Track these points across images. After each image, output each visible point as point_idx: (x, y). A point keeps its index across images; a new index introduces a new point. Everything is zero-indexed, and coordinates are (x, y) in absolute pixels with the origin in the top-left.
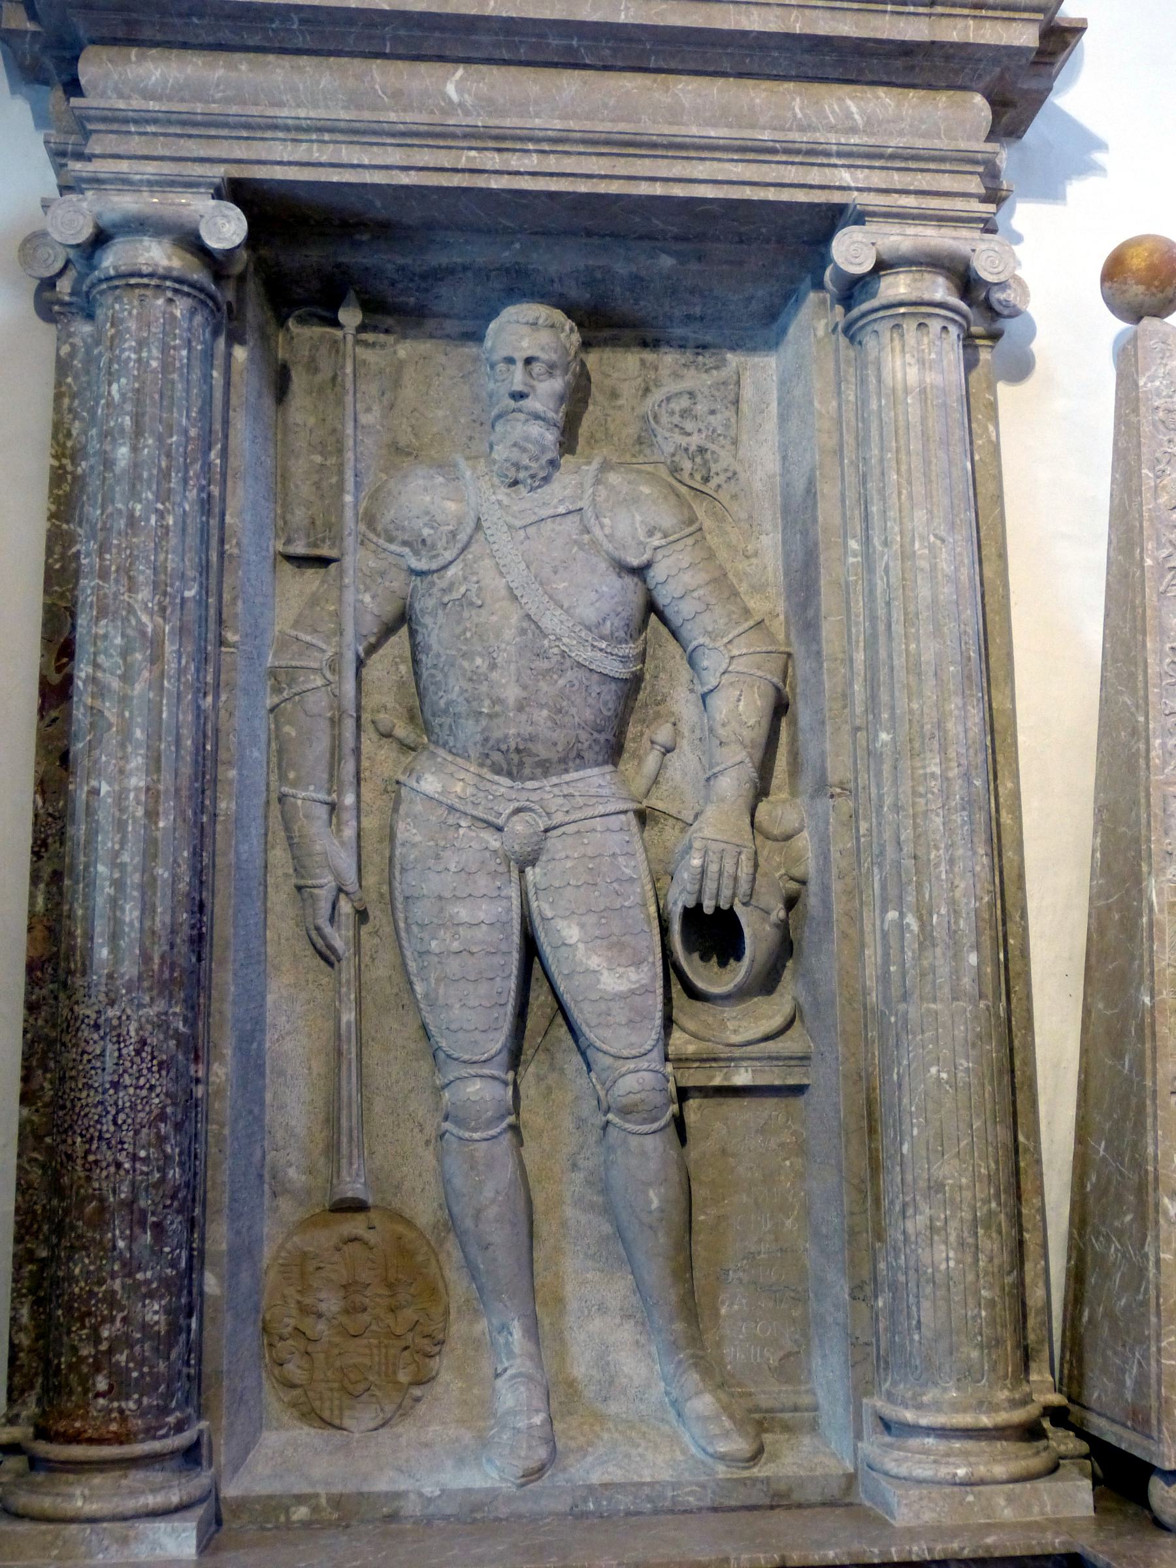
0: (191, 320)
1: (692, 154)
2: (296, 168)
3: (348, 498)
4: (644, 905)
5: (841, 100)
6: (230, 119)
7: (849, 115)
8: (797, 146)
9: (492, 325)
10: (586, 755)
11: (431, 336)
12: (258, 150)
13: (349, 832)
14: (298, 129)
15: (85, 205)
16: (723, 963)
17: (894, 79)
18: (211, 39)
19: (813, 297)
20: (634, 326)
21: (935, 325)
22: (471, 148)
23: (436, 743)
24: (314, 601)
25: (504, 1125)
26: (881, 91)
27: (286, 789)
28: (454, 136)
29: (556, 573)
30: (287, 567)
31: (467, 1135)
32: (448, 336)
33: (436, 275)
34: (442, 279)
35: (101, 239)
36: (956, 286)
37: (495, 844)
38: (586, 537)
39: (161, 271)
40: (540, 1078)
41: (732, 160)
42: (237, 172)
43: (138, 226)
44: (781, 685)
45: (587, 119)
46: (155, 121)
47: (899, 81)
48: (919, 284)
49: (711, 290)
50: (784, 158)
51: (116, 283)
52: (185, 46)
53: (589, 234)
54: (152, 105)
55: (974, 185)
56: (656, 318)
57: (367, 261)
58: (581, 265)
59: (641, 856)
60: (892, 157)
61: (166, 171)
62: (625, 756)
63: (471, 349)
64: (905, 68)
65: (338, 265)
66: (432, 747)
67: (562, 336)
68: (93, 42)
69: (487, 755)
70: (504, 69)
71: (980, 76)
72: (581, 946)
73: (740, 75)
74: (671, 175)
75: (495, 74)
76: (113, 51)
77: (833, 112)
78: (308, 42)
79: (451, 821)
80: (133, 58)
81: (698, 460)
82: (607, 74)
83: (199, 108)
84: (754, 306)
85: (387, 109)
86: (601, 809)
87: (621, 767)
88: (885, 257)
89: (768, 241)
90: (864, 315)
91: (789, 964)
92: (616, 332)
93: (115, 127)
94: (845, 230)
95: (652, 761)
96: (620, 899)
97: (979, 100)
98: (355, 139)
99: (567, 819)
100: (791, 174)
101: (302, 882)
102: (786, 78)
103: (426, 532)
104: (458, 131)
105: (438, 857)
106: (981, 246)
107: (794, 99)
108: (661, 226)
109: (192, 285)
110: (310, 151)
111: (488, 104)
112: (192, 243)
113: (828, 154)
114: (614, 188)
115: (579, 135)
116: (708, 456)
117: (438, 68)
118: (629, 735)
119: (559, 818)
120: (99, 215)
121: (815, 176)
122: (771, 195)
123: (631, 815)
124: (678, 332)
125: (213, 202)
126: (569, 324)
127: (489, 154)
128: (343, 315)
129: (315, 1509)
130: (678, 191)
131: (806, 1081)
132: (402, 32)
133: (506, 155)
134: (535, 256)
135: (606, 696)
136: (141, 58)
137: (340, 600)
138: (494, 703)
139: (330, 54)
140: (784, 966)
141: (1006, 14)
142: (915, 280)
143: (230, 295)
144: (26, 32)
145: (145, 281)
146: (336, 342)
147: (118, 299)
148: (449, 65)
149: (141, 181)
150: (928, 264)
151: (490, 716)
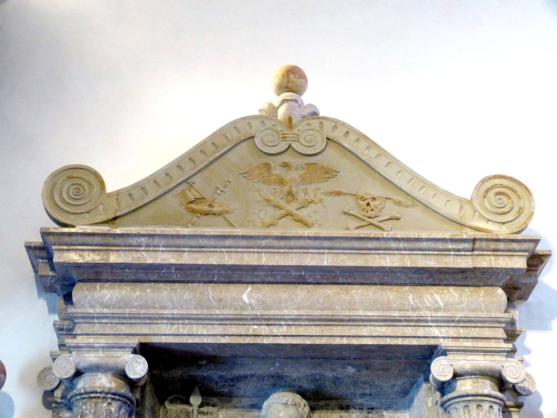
0: (119, 412)
1: (361, 323)
2: (171, 337)
5: (432, 295)
6: (142, 316)
7: (436, 302)
8: (411, 318)
9: (265, 404)
11: (236, 407)
12: (154, 329)
14: (173, 319)
15: (71, 358)
17: (457, 283)
18: (134, 278)
19: (425, 386)
20: (336, 399)
21: (486, 406)
22: (254, 325)
26: (451, 289)
28: (246, 320)
32: (244, 407)
33: (238, 379)
34: (240, 381)
35: (78, 373)
36: (497, 384)
39: (106, 390)
41: (380, 326)
42: (144, 340)
43: (96, 368)
45: (310, 309)
46: (107, 318)
47: (460, 284)
48: (476, 385)
49: (374, 382)
50: (405, 324)
51: (84, 396)
52: (122, 281)
53: (312, 358)
54: (106, 311)
55: (501, 334)
56: (347, 395)
57: (205, 374)
58: (309, 373)
60: (459, 321)
61: (110, 342)
63: (255, 413)
64: (462, 278)
65: (190, 376)
67: (300, 409)
68: (80, 281)
70: (270, 286)
71: (500, 280)
73: (382, 284)
74: (350, 334)
75: (266, 289)
76: (89, 285)
77: (428, 301)
78: (179, 277)
80: (98, 288)
82: (318, 286)
83: (127, 311)
84: (396, 389)
85: (214, 308)
88: (458, 372)
89: (401, 358)
90: (450, 400)
92: (327, 402)
93: (88, 320)
94: (437, 359)
97: (500, 291)
98: (200, 322)
100: (409, 331)
102: (405, 285)
104: (249, 317)
106: (506, 365)
107: (409, 295)
108: (347, 354)
109: (120, 395)
110: (178, 328)
111: (263, 304)
112: (122, 375)
113: (427, 321)
114: (323, 341)
115: (305, 317)
117: (239, 287)
120: (78, 364)
121: (421, 332)
122: (400, 342)
124: (359, 401)
125: (132, 355)
126: (304, 402)
127: (263, 327)
128: (192, 400)
130: (355, 342)
132: (222, 272)
133: (271, 327)
134: (286, 369)
136: (102, 288)
139: (188, 282)
141: (509, 253)
142: (474, 382)
143: (138, 395)
144: (49, 276)
145: (98, 395)
146: (188, 413)
147: (84, 404)
148: (244, 285)
149: (99, 347)
150: (480, 375)
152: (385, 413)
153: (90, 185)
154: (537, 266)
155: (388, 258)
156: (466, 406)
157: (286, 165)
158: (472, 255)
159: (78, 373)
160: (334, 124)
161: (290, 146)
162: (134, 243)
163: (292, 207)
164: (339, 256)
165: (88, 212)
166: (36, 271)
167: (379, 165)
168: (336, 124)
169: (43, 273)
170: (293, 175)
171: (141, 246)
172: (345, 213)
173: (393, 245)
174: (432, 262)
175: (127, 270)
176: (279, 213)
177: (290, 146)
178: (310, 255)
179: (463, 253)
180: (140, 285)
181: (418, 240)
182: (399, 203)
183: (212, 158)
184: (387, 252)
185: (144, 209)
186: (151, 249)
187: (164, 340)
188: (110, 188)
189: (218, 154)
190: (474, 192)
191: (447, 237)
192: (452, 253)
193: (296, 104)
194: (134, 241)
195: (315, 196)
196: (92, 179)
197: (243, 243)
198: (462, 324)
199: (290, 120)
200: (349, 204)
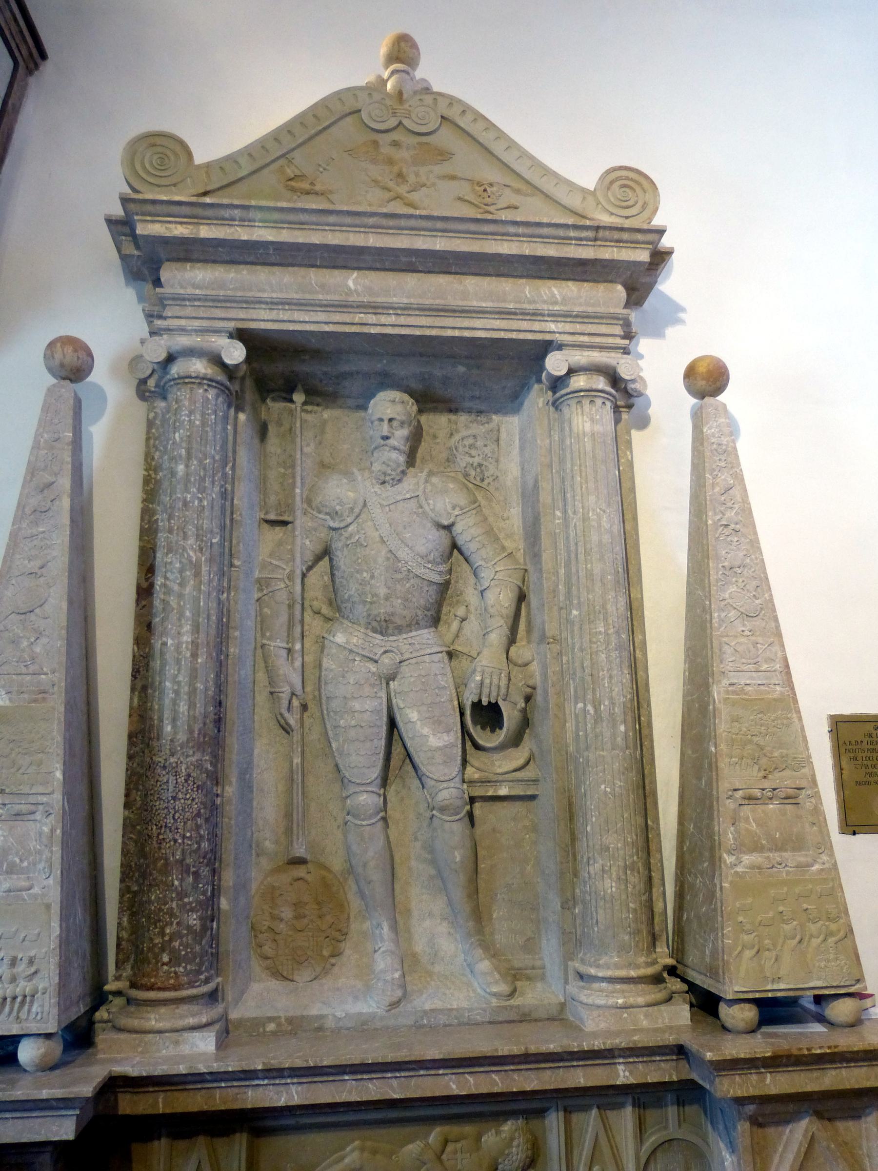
0: (216, 400)
1: (474, 315)
3: (298, 491)
4: (452, 701)
5: (549, 288)
7: (554, 296)
10: (421, 623)
11: (341, 407)
12: (253, 314)
13: (298, 663)
14: (272, 303)
15: (162, 342)
16: (493, 731)
18: (228, 258)
19: (536, 386)
21: (599, 402)
22: (361, 313)
23: (343, 617)
24: (280, 544)
25: (379, 817)
26: (570, 283)
27: (265, 642)
28: (352, 307)
29: (405, 528)
30: (266, 526)
31: (359, 822)
33: (344, 376)
35: (171, 359)
37: (374, 670)
38: (420, 510)
39: (201, 375)
40: (397, 792)
42: (241, 325)
43: (190, 352)
44: (521, 585)
46: (199, 300)
51: (179, 381)
52: (214, 262)
53: (421, 355)
54: (197, 292)
55: (618, 330)
59: (450, 675)
60: (577, 316)
62: (441, 623)
63: (362, 414)
65: (293, 372)
66: (341, 619)
68: (168, 260)
69: (370, 623)
70: (377, 272)
72: (418, 722)
73: (498, 275)
76: (179, 265)
77: (545, 294)
79: (351, 657)
80: (188, 268)
81: (478, 470)
83: (222, 293)
86: (429, 651)
87: (439, 628)
90: (562, 396)
91: (527, 731)
92: (435, 404)
93: (179, 302)
95: (455, 625)
96: (439, 698)
97: (620, 287)
99: (411, 656)
100: (525, 325)
101: (273, 690)
102: (521, 277)
103: (338, 508)
104: (354, 304)
105: (344, 677)
106: (622, 361)
109: (217, 382)
110: (278, 314)
112: (217, 360)
113: (543, 315)
115: (416, 306)
116: (483, 468)
118: (443, 612)
119: (406, 656)
120: (169, 347)
121: (537, 326)
122: (514, 336)
123: (444, 654)
125: (229, 340)
126: (411, 401)
129: (279, 1025)
130: (467, 334)
131: (537, 793)
132: (326, 255)
133: (378, 316)
135: (431, 592)
137: (293, 543)
138: (373, 596)
140: (525, 732)
141: (633, 245)
145: (193, 380)
147: (179, 390)
149: (192, 330)
151: (371, 603)
152: (494, 417)
153: (176, 154)
154: (658, 264)
155: (506, 244)
156: (579, 402)
157: (396, 144)
158: (594, 246)
159: (171, 359)
160: (450, 101)
161: (400, 123)
162: (227, 215)
163: (402, 190)
164: (453, 240)
165: (175, 185)
166: (119, 250)
167: (498, 149)
168: (452, 101)
169: (128, 252)
170: (404, 154)
171: (235, 220)
172: (460, 199)
173: (512, 229)
174: (551, 251)
175: (220, 249)
176: (387, 195)
177: (400, 123)
178: (422, 238)
179: (585, 243)
180: (236, 266)
181: (539, 225)
182: (518, 191)
183: (313, 132)
184: (505, 238)
185: (239, 185)
186: (246, 223)
187: (263, 326)
188: (200, 158)
189: (320, 128)
190: (598, 183)
191: (570, 223)
192: (573, 242)
193: (407, 77)
194: (227, 213)
195: (428, 179)
196: (178, 148)
197: (348, 220)
198: (579, 320)
199: (400, 93)
200: (464, 190)
